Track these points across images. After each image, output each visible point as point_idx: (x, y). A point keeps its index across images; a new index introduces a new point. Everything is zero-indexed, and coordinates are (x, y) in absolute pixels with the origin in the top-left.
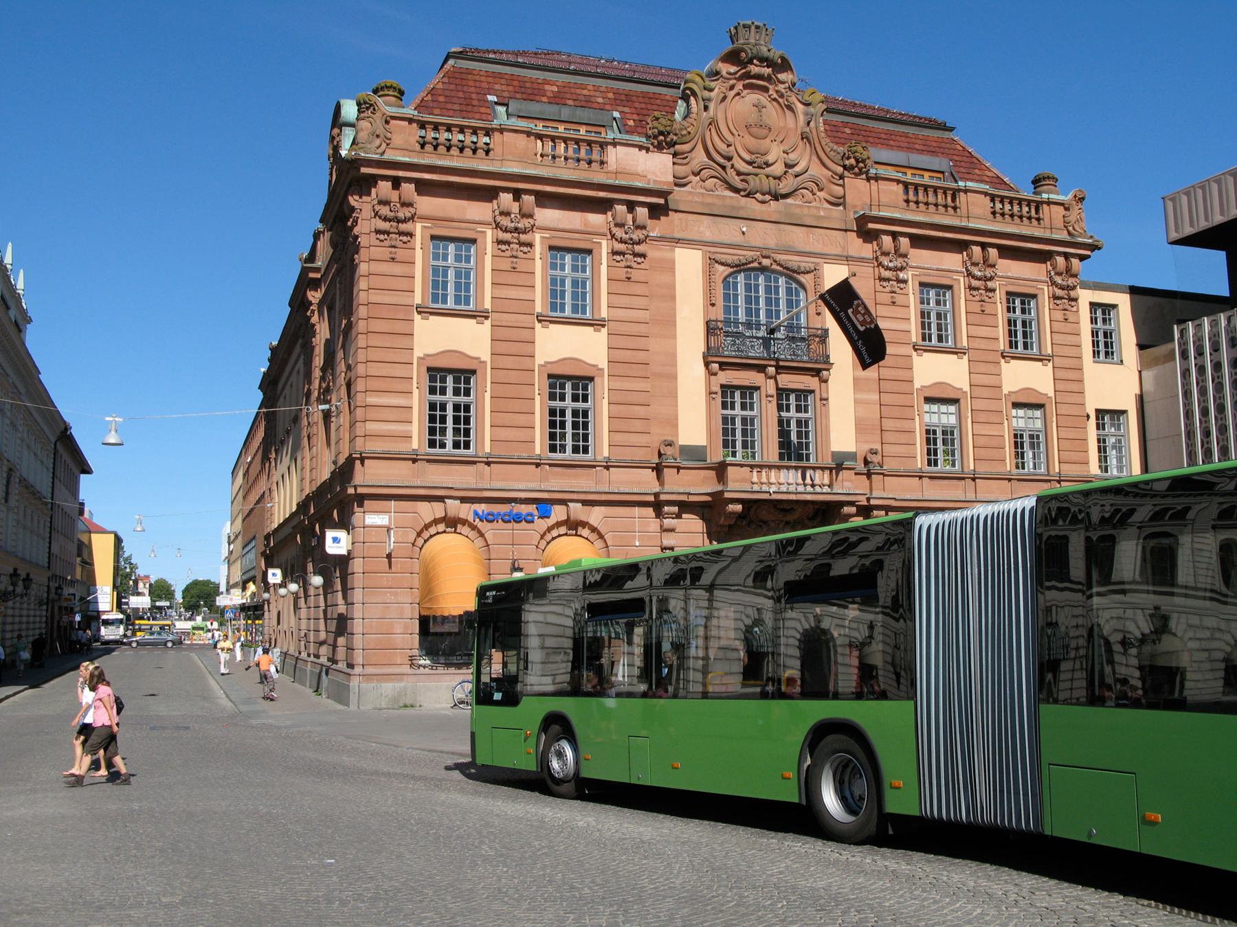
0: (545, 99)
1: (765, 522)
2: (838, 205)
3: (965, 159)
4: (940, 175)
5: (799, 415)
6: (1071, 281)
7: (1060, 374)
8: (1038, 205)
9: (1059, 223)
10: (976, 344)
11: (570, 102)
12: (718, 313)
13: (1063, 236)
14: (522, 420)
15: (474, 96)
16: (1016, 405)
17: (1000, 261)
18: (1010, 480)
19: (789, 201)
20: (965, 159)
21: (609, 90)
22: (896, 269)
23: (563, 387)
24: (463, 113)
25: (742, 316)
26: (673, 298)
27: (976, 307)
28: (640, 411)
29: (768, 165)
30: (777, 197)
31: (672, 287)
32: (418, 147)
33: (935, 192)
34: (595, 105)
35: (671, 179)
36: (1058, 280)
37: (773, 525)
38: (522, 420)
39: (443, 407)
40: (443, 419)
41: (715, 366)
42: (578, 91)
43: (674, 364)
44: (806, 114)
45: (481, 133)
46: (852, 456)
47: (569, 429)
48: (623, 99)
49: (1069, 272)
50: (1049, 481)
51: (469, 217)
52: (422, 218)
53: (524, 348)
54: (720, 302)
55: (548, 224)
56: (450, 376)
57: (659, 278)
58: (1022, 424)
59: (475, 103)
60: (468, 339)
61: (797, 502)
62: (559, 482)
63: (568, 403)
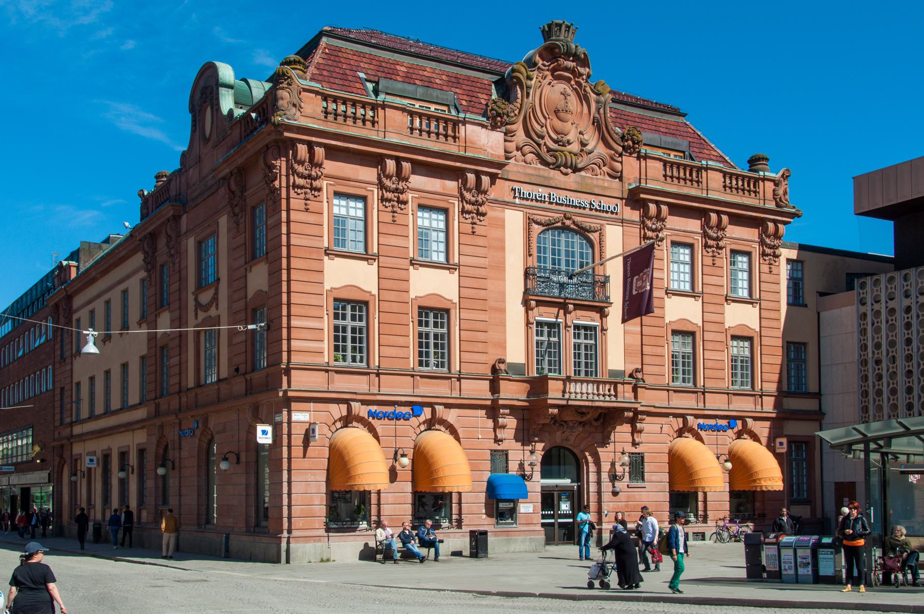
0: (399, 78)
1: (565, 422)
2: (615, 178)
3: (696, 141)
4: (682, 155)
5: (586, 341)
6: (776, 242)
7: (465, 282)
8: (756, 180)
9: (769, 195)
10: (465, 260)
11: (417, 82)
12: (533, 262)
13: (771, 205)
14: (401, 341)
15: (348, 72)
16: (734, 337)
17: (729, 226)
18: (327, 371)
19: (583, 173)
20: (696, 141)
21: (443, 73)
22: (396, 190)
23: (344, 308)
24: (343, 87)
25: (549, 266)
26: (503, 249)
27: (387, 217)
28: (481, 336)
29: (569, 143)
30: (576, 170)
31: (503, 240)
32: (322, 116)
33: (678, 168)
34: (435, 86)
35: (502, 153)
36: (468, 196)
37: (571, 424)
38: (401, 341)
39: (344, 329)
40: (344, 339)
41: (533, 303)
42: (421, 72)
43: (504, 301)
44: (598, 102)
45: (359, 106)
46: (621, 373)
47: (432, 350)
48: (455, 81)
49: (777, 235)
50: (368, 374)
51: (361, 178)
52: (327, 176)
53: (402, 285)
54: (534, 251)
55: (417, 186)
56: (351, 306)
57: (494, 233)
58: (735, 351)
59: (350, 78)
60: (360, 277)
61: (592, 407)
62: (428, 389)
63: (348, 323)
